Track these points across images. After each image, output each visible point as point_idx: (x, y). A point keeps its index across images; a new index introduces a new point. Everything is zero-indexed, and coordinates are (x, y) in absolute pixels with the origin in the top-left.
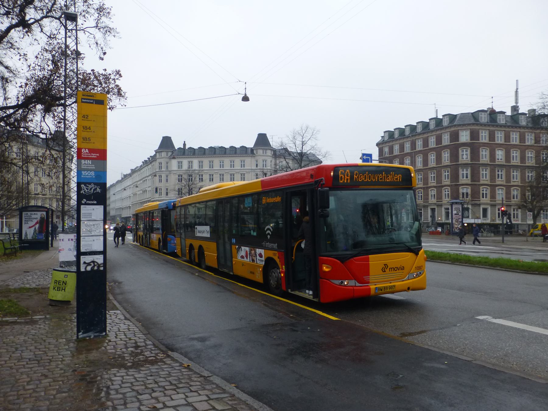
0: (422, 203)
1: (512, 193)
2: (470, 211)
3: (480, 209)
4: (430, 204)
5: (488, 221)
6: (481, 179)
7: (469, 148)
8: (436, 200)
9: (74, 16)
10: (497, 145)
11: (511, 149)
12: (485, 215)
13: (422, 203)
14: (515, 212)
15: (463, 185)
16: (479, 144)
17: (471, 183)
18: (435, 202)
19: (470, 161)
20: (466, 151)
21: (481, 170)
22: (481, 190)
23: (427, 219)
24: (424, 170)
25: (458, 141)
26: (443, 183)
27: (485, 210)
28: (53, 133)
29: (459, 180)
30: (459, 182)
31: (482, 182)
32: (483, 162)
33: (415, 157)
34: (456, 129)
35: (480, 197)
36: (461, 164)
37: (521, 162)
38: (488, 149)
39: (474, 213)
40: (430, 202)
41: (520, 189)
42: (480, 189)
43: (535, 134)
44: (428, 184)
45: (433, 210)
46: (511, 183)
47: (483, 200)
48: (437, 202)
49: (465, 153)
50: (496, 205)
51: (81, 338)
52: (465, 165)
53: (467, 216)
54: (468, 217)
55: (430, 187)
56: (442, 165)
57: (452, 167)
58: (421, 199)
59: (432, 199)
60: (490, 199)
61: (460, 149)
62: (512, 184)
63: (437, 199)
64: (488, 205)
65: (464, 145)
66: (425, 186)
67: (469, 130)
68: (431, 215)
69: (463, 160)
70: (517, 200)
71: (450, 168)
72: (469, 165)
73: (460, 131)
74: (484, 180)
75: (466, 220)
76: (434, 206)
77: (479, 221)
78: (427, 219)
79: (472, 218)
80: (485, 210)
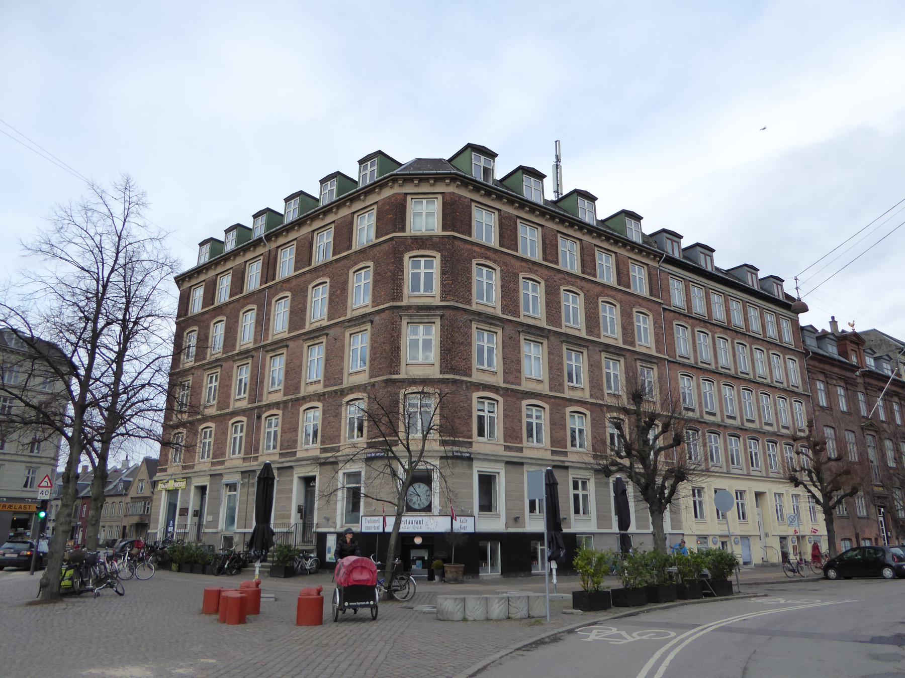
0: (276, 458)
1: (569, 424)
2: (436, 485)
3: (471, 475)
4: (298, 460)
5: (495, 524)
6: (475, 365)
7: (438, 255)
8: (318, 445)
9: (352, 491)
10: (524, 264)
11: (561, 284)
12: (487, 506)
13: (276, 458)
14: (580, 492)
15: (413, 382)
16: (468, 246)
17: (439, 376)
18: (317, 453)
19: (438, 298)
20: (429, 265)
21: (475, 333)
22: (475, 405)
23: (285, 521)
24: (291, 344)
25: (403, 229)
26: (345, 382)
27: (487, 482)
28: (131, 464)
29: (398, 366)
30: (398, 373)
31: (476, 377)
32: (481, 309)
33: (269, 304)
34: (397, 190)
35: (470, 430)
36: (408, 308)
37: (590, 331)
38: (498, 270)
39: (449, 496)
40: (299, 455)
41: (588, 413)
42: (470, 400)
43: (616, 256)
44: (297, 388)
45: (308, 481)
46: (563, 393)
47: (480, 445)
48: (324, 450)
49: (422, 271)
50: (522, 464)
51: (848, 405)
52: (423, 312)
53: (426, 504)
54: (428, 509)
55: (305, 399)
56: (348, 316)
57: (377, 319)
58: (274, 448)
59: (307, 443)
60: (505, 441)
61: (406, 256)
62: (567, 394)
63: (323, 443)
64: (496, 461)
65: (421, 242)
66: (290, 397)
67: (440, 197)
68: (302, 502)
69: (417, 294)
70: (581, 450)
71: (372, 322)
72: (438, 312)
73: (409, 198)
74: (484, 370)
75: (421, 522)
76: (309, 468)
77: (465, 525)
78: (285, 521)
79: (441, 515)
80: (487, 482)
